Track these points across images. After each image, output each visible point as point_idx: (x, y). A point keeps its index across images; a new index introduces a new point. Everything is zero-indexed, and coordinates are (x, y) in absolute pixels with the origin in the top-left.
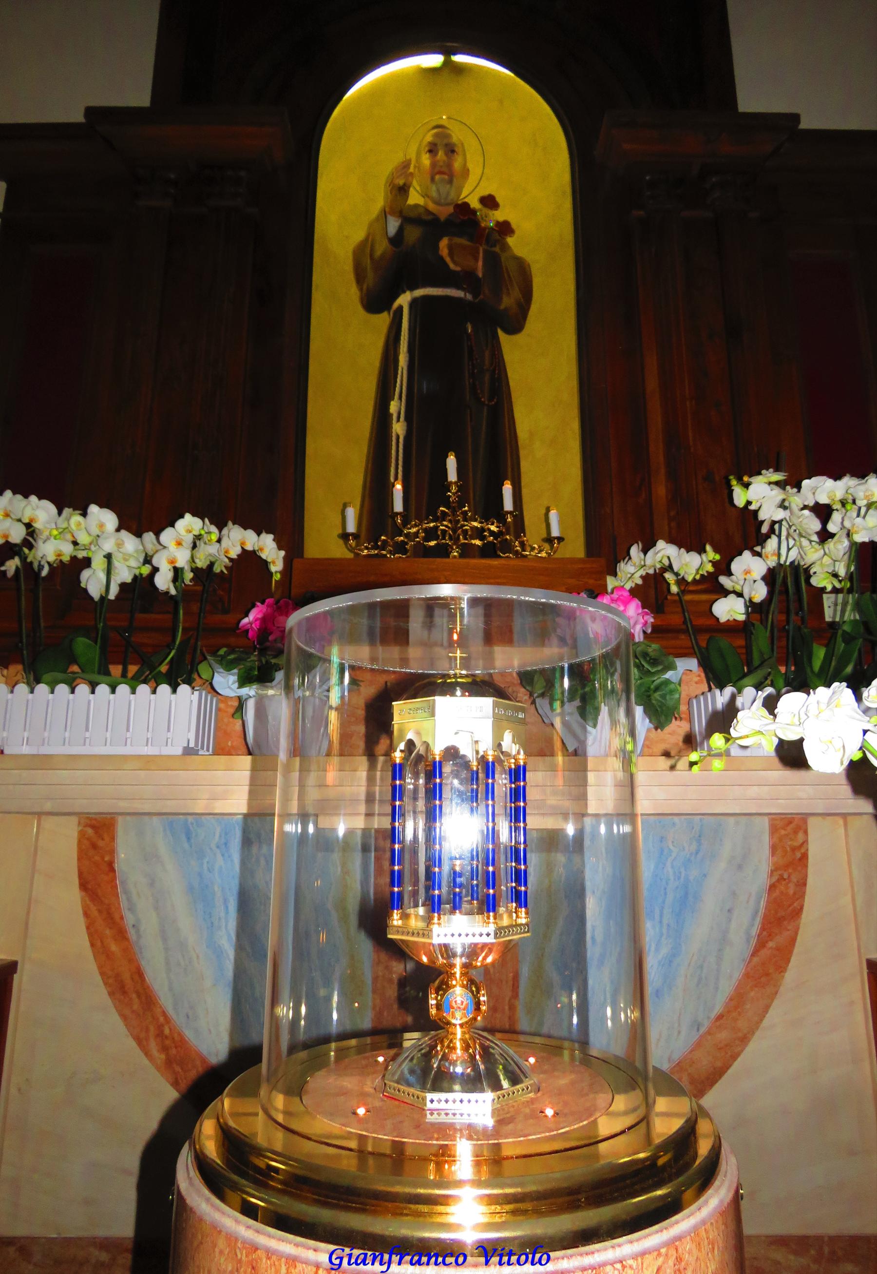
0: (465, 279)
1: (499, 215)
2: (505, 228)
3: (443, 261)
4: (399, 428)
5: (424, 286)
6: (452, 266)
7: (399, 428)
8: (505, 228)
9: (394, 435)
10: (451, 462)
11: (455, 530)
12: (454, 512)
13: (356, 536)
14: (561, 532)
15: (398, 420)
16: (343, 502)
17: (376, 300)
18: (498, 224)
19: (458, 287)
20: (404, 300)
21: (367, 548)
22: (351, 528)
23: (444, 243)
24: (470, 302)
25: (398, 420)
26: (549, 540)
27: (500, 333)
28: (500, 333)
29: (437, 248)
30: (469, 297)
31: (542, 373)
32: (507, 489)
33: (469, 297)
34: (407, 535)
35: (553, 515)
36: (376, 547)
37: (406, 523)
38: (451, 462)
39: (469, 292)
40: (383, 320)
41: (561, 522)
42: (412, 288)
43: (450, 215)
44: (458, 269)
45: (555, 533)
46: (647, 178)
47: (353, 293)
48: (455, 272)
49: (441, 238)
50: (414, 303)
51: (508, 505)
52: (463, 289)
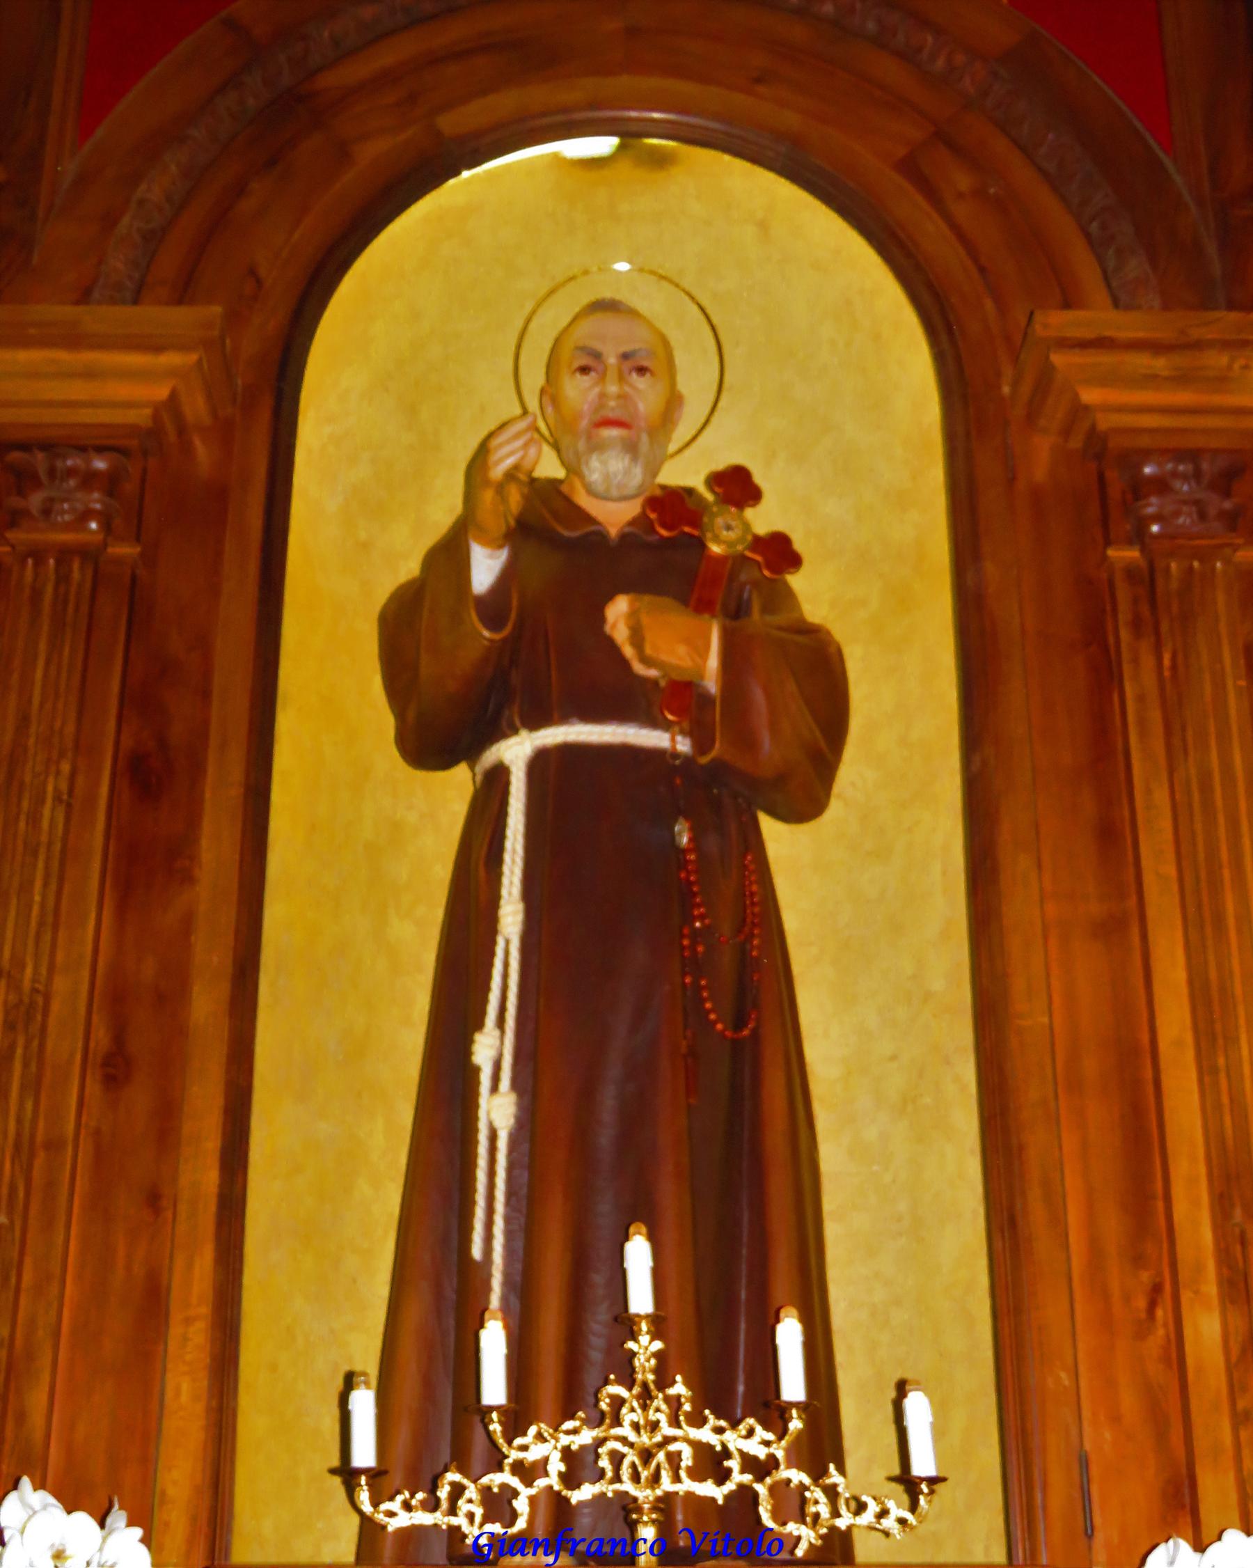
0: (678, 699)
1: (762, 519)
2: (779, 552)
3: (620, 682)
4: (498, 1110)
5: (564, 719)
6: (639, 668)
7: (498, 1110)
8: (779, 552)
9: (483, 1127)
10: (638, 1255)
11: (647, 1455)
12: (646, 1398)
13: (375, 1475)
14: (938, 1465)
15: (494, 1088)
16: (347, 1368)
17: (439, 732)
18: (759, 543)
19: (653, 722)
20: (515, 751)
21: (407, 1506)
22: (364, 1454)
23: (618, 610)
24: (688, 761)
25: (494, 1088)
26: (909, 1483)
27: (767, 824)
28: (767, 824)
29: (599, 618)
30: (684, 746)
31: (868, 903)
32: (789, 1335)
33: (684, 746)
34: (519, 1469)
35: (917, 1408)
36: (432, 1505)
37: (515, 1427)
38: (638, 1255)
39: (682, 732)
40: (456, 786)
41: (939, 1432)
42: (536, 721)
43: (633, 523)
44: (652, 673)
45: (923, 1465)
46: (1147, 470)
47: (379, 720)
48: (645, 680)
49: (610, 597)
50: (540, 762)
51: (793, 1386)
52: (665, 726)
